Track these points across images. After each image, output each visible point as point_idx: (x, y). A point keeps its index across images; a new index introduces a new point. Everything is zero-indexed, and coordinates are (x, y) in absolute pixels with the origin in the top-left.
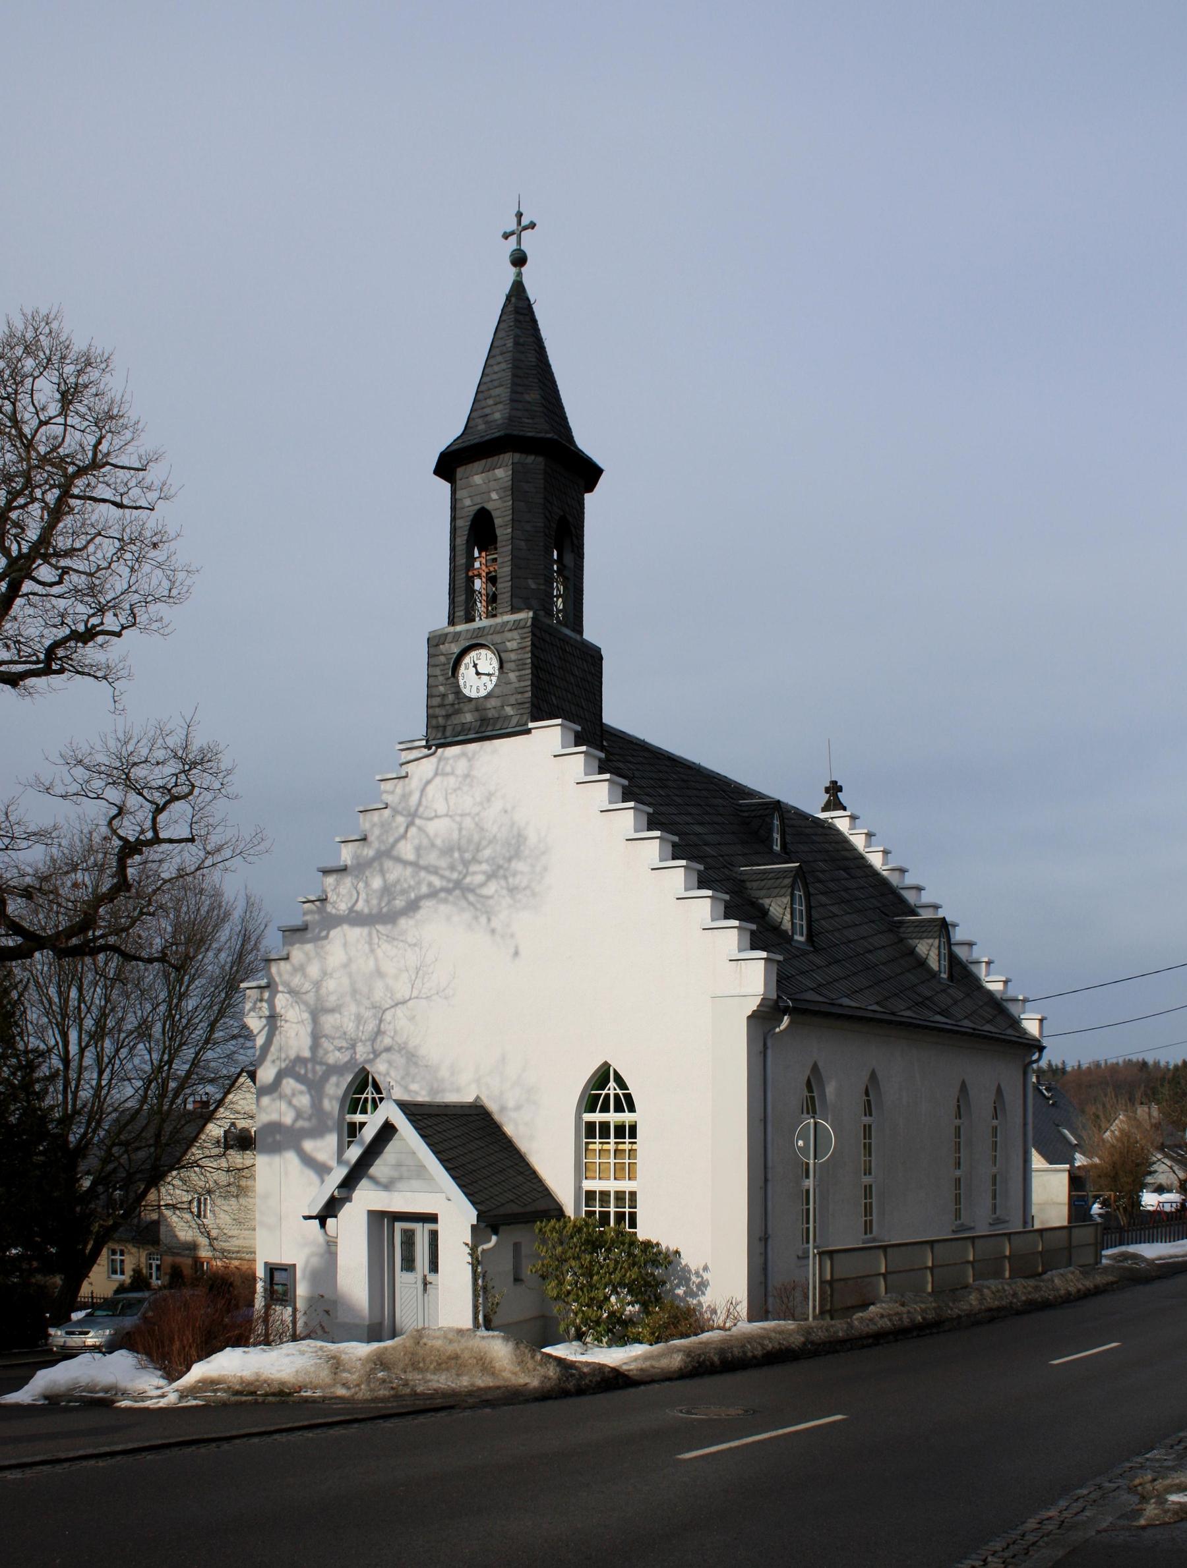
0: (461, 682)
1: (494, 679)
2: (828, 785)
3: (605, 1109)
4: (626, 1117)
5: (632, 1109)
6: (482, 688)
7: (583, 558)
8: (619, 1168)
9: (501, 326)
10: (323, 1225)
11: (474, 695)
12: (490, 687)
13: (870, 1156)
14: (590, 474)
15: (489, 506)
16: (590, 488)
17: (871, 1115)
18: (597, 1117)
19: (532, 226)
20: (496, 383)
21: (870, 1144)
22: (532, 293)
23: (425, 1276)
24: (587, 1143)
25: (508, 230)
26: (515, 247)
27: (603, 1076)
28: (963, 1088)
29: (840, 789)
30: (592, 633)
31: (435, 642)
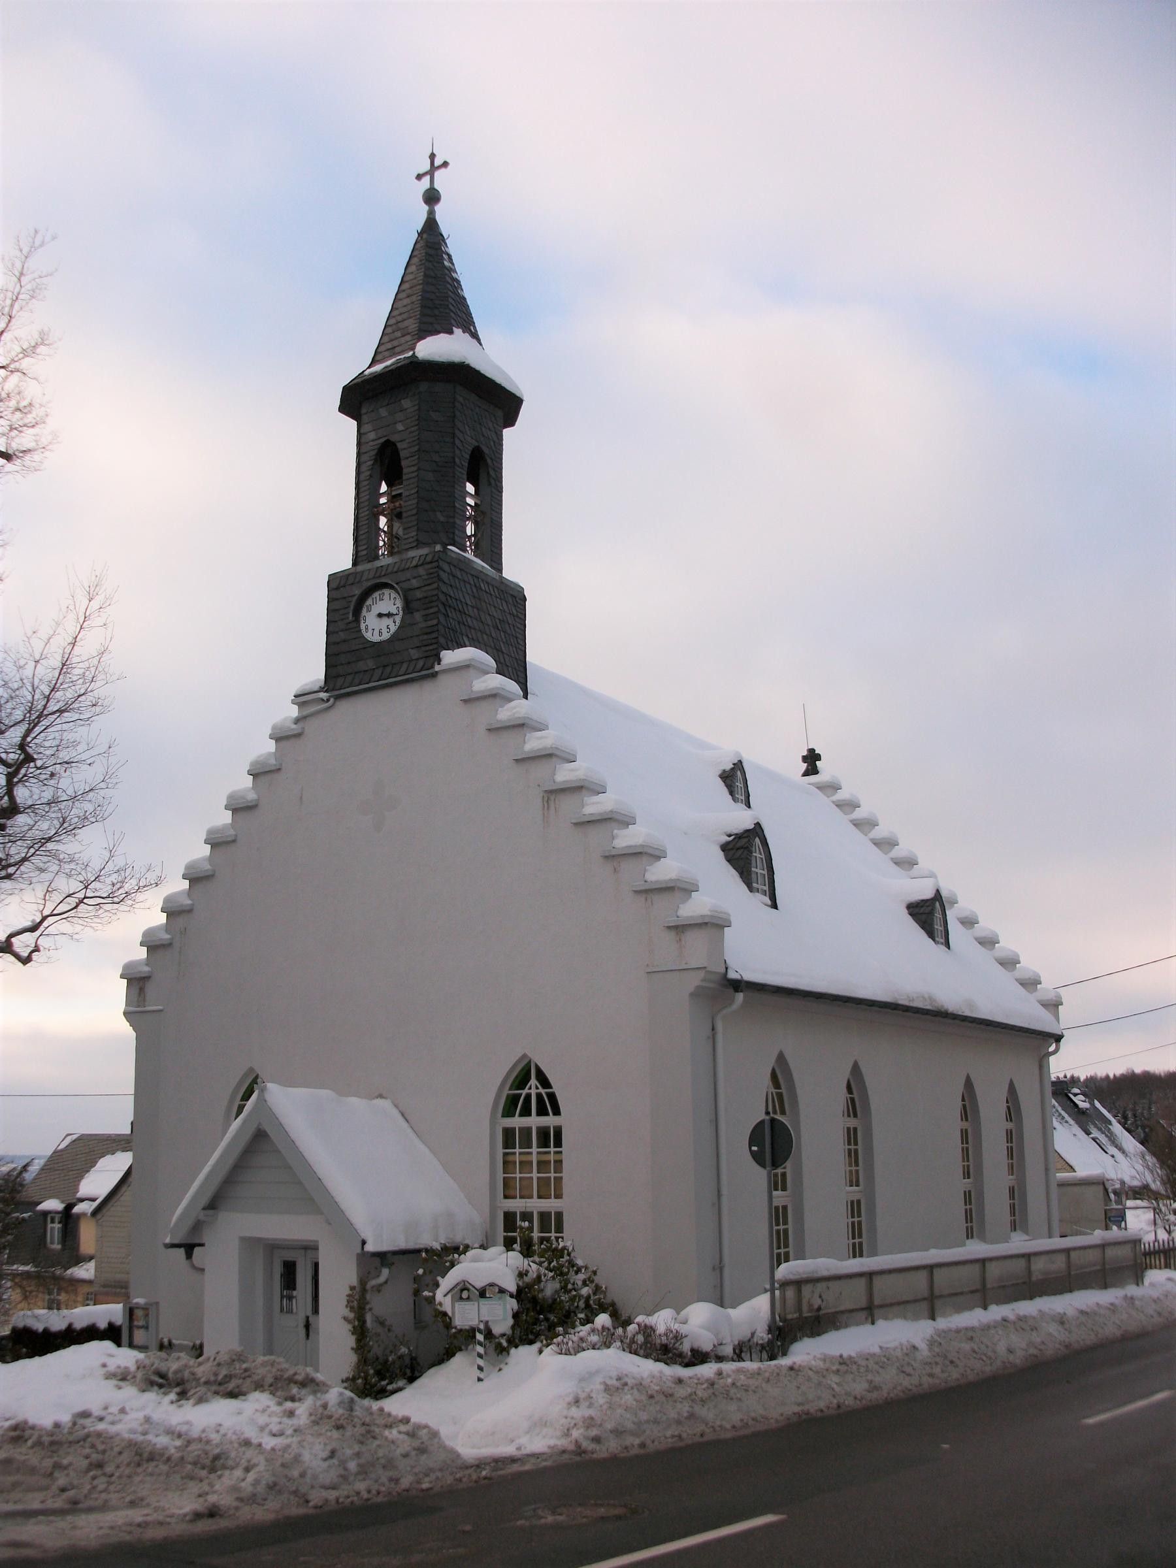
0: (363, 626)
1: (398, 619)
2: (805, 753)
3: (526, 1112)
4: (550, 1121)
5: (557, 1112)
6: (384, 631)
7: (501, 492)
8: (544, 1183)
9: (413, 261)
10: (189, 1255)
11: (376, 638)
12: (393, 629)
13: (857, 1164)
14: (504, 405)
15: (393, 438)
16: (510, 420)
17: (855, 1116)
18: (517, 1122)
19: (445, 164)
20: (404, 316)
21: (856, 1151)
22: (445, 228)
23: (308, 1318)
24: (505, 1154)
25: (421, 172)
26: (428, 186)
27: (525, 1073)
28: (969, 1084)
29: (818, 757)
30: (513, 569)
31: (337, 584)
